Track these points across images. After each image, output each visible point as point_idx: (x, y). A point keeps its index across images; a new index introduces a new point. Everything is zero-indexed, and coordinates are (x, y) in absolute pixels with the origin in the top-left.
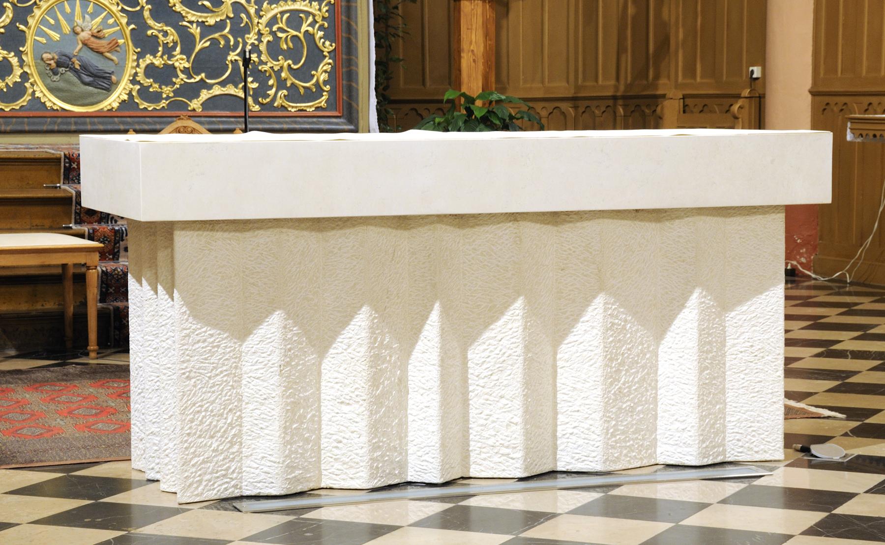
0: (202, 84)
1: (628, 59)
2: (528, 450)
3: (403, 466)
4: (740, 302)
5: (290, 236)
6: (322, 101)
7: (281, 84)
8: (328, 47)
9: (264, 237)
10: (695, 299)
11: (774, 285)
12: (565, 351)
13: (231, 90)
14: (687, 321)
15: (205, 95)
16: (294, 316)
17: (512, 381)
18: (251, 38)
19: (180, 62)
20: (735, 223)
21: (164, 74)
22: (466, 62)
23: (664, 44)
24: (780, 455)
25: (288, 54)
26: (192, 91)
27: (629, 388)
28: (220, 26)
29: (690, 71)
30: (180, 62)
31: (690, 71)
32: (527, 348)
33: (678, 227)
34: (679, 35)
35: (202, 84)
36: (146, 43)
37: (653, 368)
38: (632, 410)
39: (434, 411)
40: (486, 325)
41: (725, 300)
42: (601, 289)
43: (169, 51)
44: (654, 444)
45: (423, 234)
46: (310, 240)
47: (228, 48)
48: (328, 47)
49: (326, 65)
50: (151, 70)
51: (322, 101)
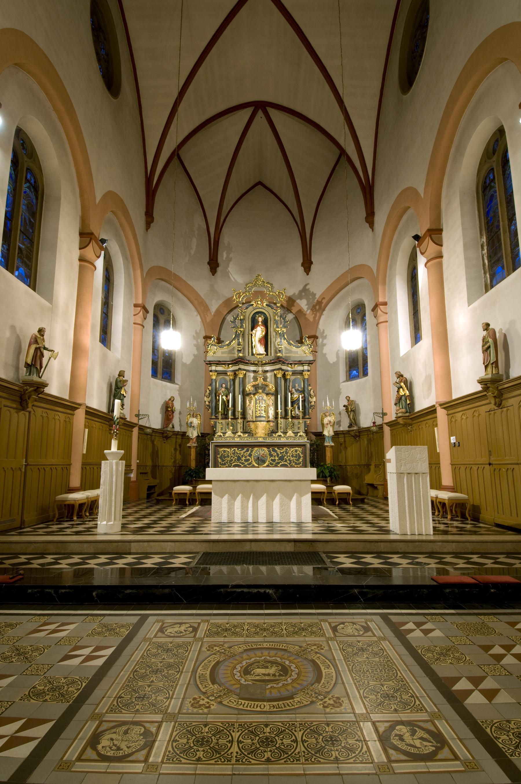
0: (280, 462)
1: (366, 458)
2: (267, 518)
3: (247, 519)
4: (304, 495)
5: (230, 482)
6: (301, 465)
7: (294, 462)
8: (302, 455)
9: (226, 483)
10: (295, 495)
11: (307, 494)
12: (274, 502)
13: (285, 463)
14: (295, 498)
15: (281, 464)
16: (230, 495)
17: (265, 506)
18: (289, 454)
19: (277, 458)
20: (302, 483)
21: (274, 460)
22: (327, 458)
23: (372, 455)
24: (311, 521)
25: (295, 457)
26: (278, 463)
27: (285, 509)
28: (283, 452)
29: (376, 460)
30: (277, 458)
31: (376, 460)
32: (267, 501)
33: (293, 483)
34: (374, 453)
35: (280, 462)
36: (271, 455)
37: (290, 506)
38: (285, 513)
39: (251, 511)
40: (261, 498)
41: (301, 495)
42: (279, 492)
43: (275, 457)
44: (290, 518)
45: (251, 483)
46: (233, 483)
47: (285, 456)
48: (302, 455)
49: (302, 458)
50: (272, 460)
51: (301, 465)
